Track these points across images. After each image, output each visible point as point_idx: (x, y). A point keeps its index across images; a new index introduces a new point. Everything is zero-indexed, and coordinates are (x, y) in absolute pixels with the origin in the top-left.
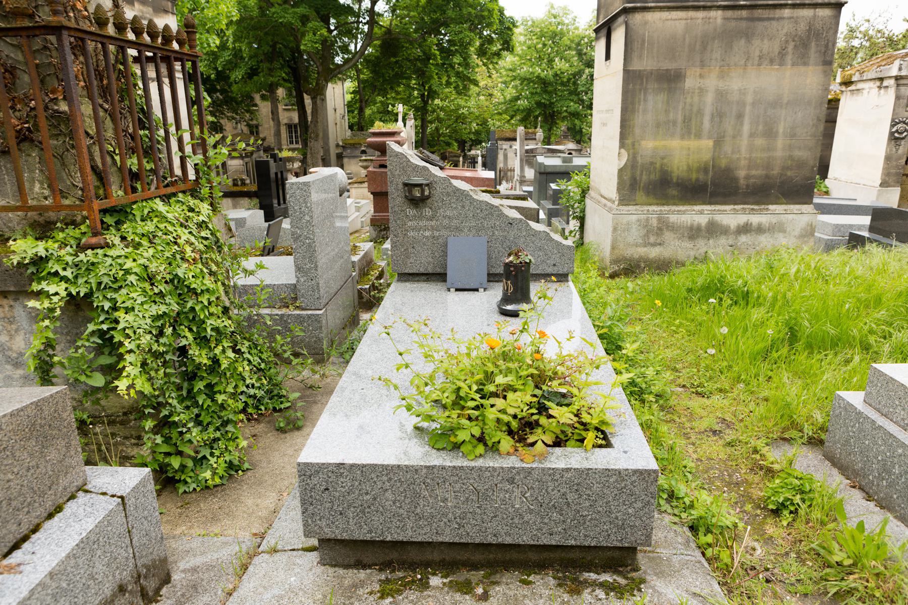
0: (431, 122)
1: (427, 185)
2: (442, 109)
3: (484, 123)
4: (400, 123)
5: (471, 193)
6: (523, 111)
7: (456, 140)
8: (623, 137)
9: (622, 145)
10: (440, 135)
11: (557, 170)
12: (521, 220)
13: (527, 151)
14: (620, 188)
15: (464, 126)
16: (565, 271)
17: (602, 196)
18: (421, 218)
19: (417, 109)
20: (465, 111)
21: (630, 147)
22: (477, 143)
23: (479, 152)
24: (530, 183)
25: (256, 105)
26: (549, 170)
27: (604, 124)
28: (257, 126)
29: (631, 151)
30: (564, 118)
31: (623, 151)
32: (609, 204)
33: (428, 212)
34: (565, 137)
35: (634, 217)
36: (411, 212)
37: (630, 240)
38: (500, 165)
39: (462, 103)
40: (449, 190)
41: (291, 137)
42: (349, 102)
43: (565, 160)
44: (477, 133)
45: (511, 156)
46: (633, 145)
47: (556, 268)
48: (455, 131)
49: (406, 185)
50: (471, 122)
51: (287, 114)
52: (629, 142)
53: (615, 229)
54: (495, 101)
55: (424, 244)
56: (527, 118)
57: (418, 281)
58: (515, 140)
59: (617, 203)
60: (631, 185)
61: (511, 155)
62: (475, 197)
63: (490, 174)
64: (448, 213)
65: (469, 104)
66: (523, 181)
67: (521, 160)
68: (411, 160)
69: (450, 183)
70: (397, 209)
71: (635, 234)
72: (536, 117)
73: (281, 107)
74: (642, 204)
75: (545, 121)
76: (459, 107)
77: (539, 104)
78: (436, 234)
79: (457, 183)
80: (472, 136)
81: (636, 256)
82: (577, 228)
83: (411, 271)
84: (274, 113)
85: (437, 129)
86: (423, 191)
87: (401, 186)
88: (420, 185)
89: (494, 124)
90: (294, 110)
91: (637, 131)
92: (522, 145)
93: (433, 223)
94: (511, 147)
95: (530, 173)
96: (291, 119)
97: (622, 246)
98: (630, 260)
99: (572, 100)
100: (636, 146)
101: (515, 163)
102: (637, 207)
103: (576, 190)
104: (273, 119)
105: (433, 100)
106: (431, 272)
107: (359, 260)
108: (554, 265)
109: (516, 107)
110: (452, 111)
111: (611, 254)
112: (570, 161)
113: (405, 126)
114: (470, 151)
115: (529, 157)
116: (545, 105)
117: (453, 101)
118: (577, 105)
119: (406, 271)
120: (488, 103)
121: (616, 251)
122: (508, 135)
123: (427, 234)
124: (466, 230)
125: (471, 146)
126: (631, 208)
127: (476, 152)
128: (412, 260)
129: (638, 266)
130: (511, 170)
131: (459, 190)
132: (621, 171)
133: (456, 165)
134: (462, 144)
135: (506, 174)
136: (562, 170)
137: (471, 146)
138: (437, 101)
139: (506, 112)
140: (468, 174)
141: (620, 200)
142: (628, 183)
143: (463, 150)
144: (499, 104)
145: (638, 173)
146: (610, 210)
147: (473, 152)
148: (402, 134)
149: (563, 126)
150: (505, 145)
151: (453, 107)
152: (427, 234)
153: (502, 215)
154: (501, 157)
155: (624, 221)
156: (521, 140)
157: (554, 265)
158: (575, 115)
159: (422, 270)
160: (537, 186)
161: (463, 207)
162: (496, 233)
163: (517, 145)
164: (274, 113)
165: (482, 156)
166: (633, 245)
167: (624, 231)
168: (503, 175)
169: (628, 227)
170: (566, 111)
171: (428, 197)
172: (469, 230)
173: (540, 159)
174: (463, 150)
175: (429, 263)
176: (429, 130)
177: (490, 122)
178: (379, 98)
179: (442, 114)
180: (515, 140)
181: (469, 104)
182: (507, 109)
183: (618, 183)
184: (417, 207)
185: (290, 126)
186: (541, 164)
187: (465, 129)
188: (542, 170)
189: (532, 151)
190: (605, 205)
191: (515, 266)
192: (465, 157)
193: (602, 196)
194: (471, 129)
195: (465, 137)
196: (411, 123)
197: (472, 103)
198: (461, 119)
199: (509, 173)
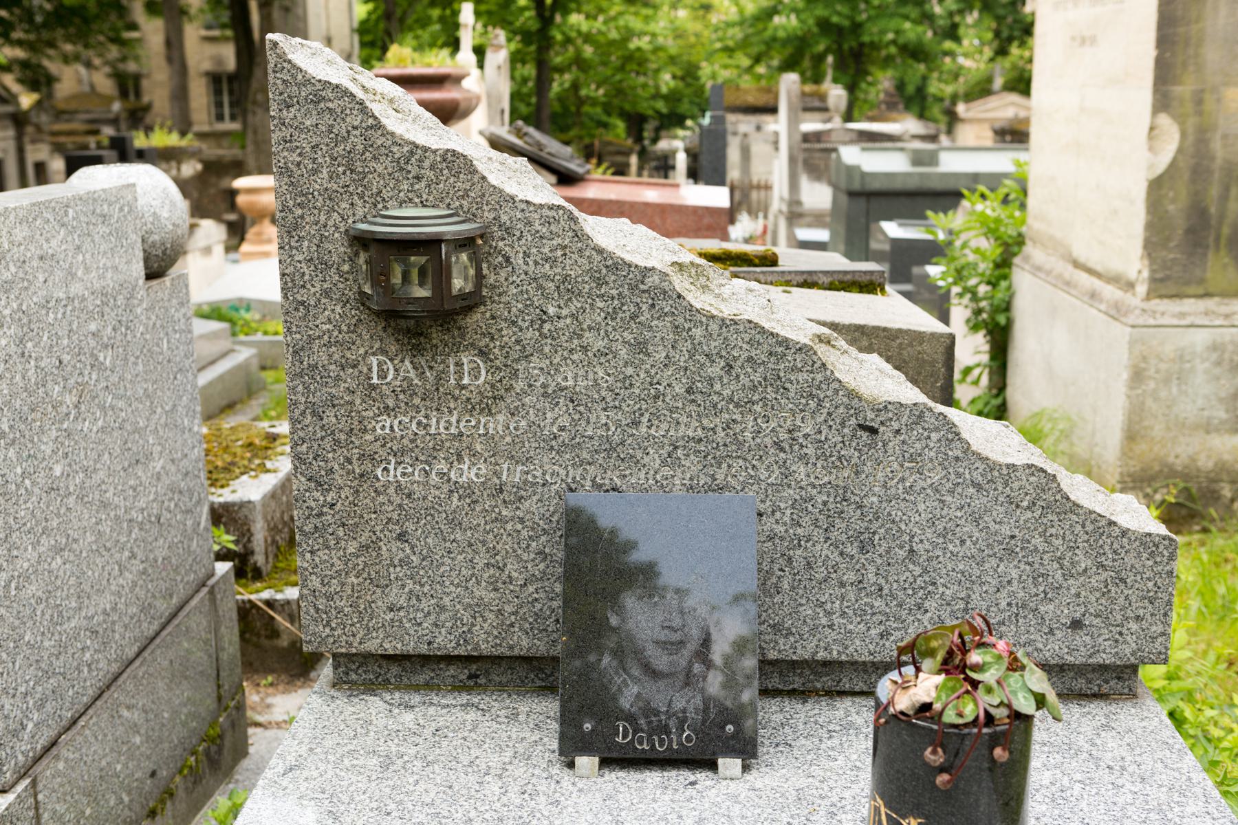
0: (561, 70)
1: (466, 243)
2: (588, 38)
3: (689, 74)
4: (466, 56)
5: (680, 283)
6: (786, 42)
7: (624, 115)
8: (1165, 74)
9: (1162, 101)
10: (581, 102)
11: (898, 185)
12: (919, 414)
13: (807, 138)
14: (1156, 237)
15: (642, 79)
16: (1127, 650)
17: (1077, 264)
18: (437, 397)
19: (527, 36)
20: (644, 43)
21: (1189, 107)
22: (673, 120)
23: (679, 144)
24: (817, 220)
25: (133, 26)
26: (876, 185)
27: (1085, 41)
28: (137, 78)
29: (1192, 122)
30: (888, 61)
31: (1164, 120)
32: (1110, 292)
33: (468, 370)
34: (891, 106)
35: (1200, 338)
36: (390, 369)
37: (1188, 409)
38: (734, 174)
39: (636, 23)
40: (575, 268)
41: (219, 105)
42: (363, 23)
43: (918, 159)
44: (673, 98)
45: (764, 152)
46: (1199, 101)
47: (1081, 639)
48: (620, 92)
49: (361, 241)
50: (657, 71)
51: (211, 50)
52: (1183, 90)
53: (1137, 376)
54: (714, 18)
55: (455, 524)
56: (797, 55)
57: (429, 686)
58: (773, 110)
59: (1142, 289)
60: (1190, 231)
61: (759, 148)
62: (698, 300)
63: (716, 197)
64: (568, 377)
65: (652, 27)
66: (795, 215)
67: (792, 160)
68: (392, 122)
69: (579, 235)
70: (321, 357)
71: (1202, 394)
72: (819, 59)
73: (192, 33)
74: (1225, 294)
75: (840, 66)
76: (629, 34)
77: (825, 26)
78: (512, 474)
79: (609, 234)
80: (661, 106)
81: (1206, 463)
82: (985, 358)
83: (390, 647)
84: (174, 45)
85: (575, 86)
86: (441, 274)
87: (338, 248)
88: (430, 244)
89: (713, 72)
90: (226, 39)
91: (1212, 55)
92: (793, 122)
93: (496, 424)
94: (758, 128)
95: (818, 196)
96: (219, 61)
97: (1158, 430)
98: (1186, 477)
99: (906, 17)
100: (1209, 105)
101: (774, 169)
102: (1210, 303)
103: (984, 244)
104: (169, 59)
105: (566, 12)
106: (485, 649)
107: (273, 495)
108: (1076, 625)
109: (768, 33)
110: (612, 43)
111: (1126, 453)
112: (932, 159)
113: (481, 65)
114: (655, 140)
115: (813, 155)
116: (839, 30)
117: (614, 19)
118: (920, 29)
119: (372, 646)
120: (697, 26)
121: (1141, 447)
122: (751, 99)
123: (468, 473)
124: (653, 459)
125: (658, 130)
126: (1189, 305)
127: (676, 144)
128: (396, 595)
129: (1213, 496)
130: (758, 187)
131: (618, 266)
132: (1156, 186)
133: (621, 170)
134: (636, 123)
135: (746, 196)
136: (912, 185)
137: (658, 130)
138: (575, 19)
139: (744, 44)
140: (652, 195)
141: (1153, 280)
142: (1180, 225)
143: (639, 139)
144: (729, 25)
145: (1214, 191)
146: (1117, 312)
147: (663, 145)
148: (466, 83)
149: (883, 81)
150: (743, 124)
151: (614, 35)
152: (468, 473)
153: (823, 388)
154: (733, 154)
155: (1169, 350)
156: (791, 109)
157: (1076, 625)
158: (915, 52)
159: (445, 642)
160: (842, 230)
161: (641, 347)
162: (801, 471)
163: (778, 125)
164: (174, 45)
165: (687, 151)
166: (1196, 427)
167: (1167, 381)
168: (745, 199)
169: (1179, 369)
170: (894, 42)
171: (471, 301)
172: (671, 460)
173: (851, 155)
174: (639, 139)
175: (477, 609)
176: (555, 88)
177: (706, 70)
178: (436, 13)
179: (588, 51)
180: (773, 110)
181: (652, 27)
182: (747, 37)
183: (1149, 226)
184: (417, 350)
185: (216, 80)
186: (852, 170)
187: (645, 86)
188: (856, 186)
189: (817, 137)
190: (1093, 295)
191: (952, 738)
192: (643, 154)
193: (1077, 264)
194: (657, 87)
195: (644, 107)
196: (498, 58)
197: (660, 25)
198: (635, 61)
199: (754, 195)
